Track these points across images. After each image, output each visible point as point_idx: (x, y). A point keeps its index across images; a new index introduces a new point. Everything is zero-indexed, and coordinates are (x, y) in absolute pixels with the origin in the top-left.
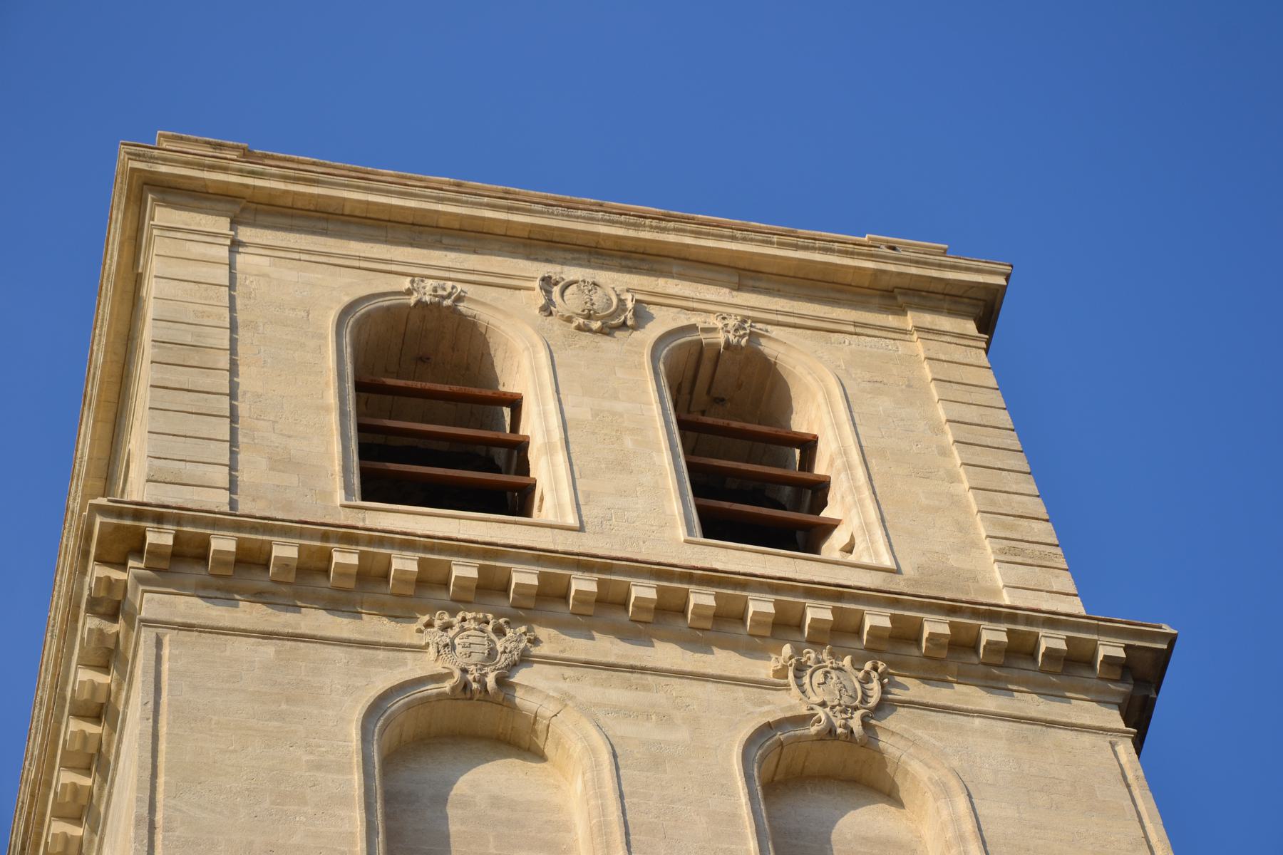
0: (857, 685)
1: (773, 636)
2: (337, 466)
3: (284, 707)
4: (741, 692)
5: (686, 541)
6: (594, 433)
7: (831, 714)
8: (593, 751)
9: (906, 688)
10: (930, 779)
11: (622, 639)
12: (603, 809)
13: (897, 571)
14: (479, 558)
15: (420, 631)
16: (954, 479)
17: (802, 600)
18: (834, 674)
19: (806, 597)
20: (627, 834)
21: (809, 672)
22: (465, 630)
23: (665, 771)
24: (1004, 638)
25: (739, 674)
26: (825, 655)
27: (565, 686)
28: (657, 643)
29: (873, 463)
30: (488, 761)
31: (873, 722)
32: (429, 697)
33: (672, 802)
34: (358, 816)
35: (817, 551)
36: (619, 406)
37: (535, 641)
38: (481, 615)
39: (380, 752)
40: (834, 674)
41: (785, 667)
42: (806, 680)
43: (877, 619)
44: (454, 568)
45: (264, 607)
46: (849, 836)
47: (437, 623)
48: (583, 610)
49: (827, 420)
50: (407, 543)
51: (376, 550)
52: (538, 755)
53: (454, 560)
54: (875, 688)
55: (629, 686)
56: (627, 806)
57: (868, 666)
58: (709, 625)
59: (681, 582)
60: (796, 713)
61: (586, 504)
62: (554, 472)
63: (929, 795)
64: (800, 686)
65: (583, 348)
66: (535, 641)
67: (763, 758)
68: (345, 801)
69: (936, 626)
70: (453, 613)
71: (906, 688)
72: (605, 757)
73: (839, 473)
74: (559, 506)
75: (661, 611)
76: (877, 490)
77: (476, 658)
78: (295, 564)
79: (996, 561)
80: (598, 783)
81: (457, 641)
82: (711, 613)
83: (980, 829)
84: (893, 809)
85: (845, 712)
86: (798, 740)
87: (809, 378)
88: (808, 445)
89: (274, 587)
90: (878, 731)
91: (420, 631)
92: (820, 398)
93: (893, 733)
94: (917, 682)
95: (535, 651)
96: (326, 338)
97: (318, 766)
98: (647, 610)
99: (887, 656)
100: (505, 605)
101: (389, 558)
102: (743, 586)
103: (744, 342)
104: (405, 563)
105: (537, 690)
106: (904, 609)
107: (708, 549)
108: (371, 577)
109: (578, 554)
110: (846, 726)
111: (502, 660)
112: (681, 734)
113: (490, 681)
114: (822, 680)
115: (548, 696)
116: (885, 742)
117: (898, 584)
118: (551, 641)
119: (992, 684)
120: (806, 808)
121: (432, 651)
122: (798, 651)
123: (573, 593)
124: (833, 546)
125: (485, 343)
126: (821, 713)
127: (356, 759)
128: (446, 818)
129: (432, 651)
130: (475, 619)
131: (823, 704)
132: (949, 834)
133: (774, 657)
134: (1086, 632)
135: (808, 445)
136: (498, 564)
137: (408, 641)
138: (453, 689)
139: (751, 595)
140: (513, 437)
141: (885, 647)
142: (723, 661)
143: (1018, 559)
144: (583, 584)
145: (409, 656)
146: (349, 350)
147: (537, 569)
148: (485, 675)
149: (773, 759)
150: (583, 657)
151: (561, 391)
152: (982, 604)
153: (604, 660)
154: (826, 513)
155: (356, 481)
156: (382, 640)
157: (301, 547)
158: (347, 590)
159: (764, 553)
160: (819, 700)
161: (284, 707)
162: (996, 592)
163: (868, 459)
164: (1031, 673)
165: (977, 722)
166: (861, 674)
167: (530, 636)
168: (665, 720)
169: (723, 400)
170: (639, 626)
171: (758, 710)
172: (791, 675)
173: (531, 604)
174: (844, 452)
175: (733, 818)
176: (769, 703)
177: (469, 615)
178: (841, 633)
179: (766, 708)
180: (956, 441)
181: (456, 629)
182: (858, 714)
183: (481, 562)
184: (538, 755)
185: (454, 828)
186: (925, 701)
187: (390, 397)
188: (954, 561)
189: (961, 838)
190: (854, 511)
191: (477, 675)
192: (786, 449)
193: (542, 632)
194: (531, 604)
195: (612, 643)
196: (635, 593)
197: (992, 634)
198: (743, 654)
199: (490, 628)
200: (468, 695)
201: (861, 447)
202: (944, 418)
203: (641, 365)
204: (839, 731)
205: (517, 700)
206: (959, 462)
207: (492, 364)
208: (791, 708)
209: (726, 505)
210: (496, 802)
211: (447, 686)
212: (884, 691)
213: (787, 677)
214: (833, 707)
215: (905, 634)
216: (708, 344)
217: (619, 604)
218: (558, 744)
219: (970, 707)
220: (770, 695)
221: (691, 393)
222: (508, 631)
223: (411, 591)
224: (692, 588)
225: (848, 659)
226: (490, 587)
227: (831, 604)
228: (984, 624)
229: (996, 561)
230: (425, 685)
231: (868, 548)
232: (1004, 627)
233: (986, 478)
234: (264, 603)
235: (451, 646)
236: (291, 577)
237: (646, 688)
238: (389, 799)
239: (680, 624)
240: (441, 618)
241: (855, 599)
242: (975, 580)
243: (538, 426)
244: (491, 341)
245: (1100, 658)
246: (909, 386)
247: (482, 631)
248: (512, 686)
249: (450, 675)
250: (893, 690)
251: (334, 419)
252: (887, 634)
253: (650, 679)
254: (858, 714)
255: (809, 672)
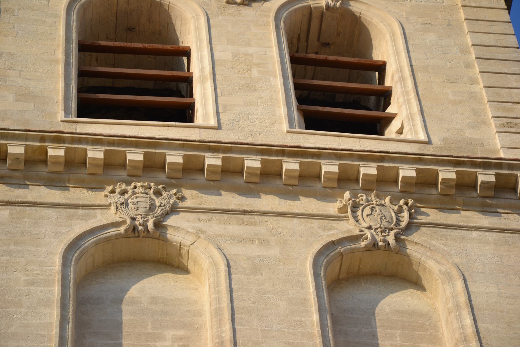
0: (393, 215)
1: (339, 187)
2: (60, 97)
3: (12, 247)
4: (316, 223)
5: (288, 132)
6: (233, 68)
7: (374, 233)
8: (215, 264)
9: (428, 215)
10: (440, 271)
11: (240, 195)
12: (219, 300)
13: (429, 142)
14: (144, 148)
15: (106, 196)
16: (473, 81)
17: (280, 158)
18: (378, 208)
19: (360, 161)
20: (233, 314)
21: (361, 208)
22: (135, 194)
23: (262, 275)
24: (493, 179)
25: (315, 212)
26: (373, 197)
27: (199, 225)
28: (263, 196)
29: (419, 76)
30: (151, 276)
31: (403, 237)
32: (110, 237)
33: (265, 293)
34: (55, 313)
35: (382, 134)
36: (251, 50)
37: (182, 199)
38: (146, 184)
39: (326, 283)
40: (378, 208)
41: (345, 206)
42: (359, 213)
43: (408, 172)
44: (88, 152)
45: (4, 186)
46: (387, 311)
47: (118, 190)
48: (214, 177)
49: (391, 51)
50: (97, 140)
51: (76, 146)
52: (183, 270)
53: (128, 150)
54: (405, 216)
55: (242, 223)
56: (234, 297)
57: (402, 202)
58: (296, 182)
59: (277, 156)
60: (351, 234)
61: (224, 112)
62: (204, 94)
63: (439, 281)
64: (355, 217)
65: (230, 15)
66: (182, 199)
67: (328, 263)
68: (48, 304)
69: (447, 174)
70: (128, 183)
71: (428, 215)
72: (223, 267)
73: (396, 84)
74: (206, 115)
75: (264, 174)
76: (420, 93)
77: (141, 211)
78: (23, 158)
79: (497, 132)
80: (216, 284)
81: (129, 201)
82: (297, 174)
83: (470, 301)
84: (418, 292)
85: (384, 231)
86: (353, 251)
87: (381, 24)
88: (381, 68)
89: (10, 173)
90: (406, 242)
91: (106, 196)
92: (388, 37)
93: (416, 243)
94: (436, 211)
95: (181, 204)
96: (59, 17)
97: (32, 283)
98: (255, 175)
99: (415, 196)
100: (162, 177)
101: (85, 150)
102: (318, 156)
103: (338, 4)
104: (96, 153)
105: (181, 229)
106: (425, 164)
107: (302, 136)
108: (74, 163)
109: (209, 142)
110: (384, 241)
111: (159, 211)
112: (274, 251)
113: (150, 225)
114: (369, 212)
115: (188, 232)
116: (412, 250)
117: (429, 150)
118: (192, 197)
119: (486, 209)
120: (356, 296)
121: (113, 207)
122: (354, 195)
123: (479, 183)
124: (391, 131)
125: (169, 16)
126: (368, 233)
127: (58, 277)
128: (121, 312)
129: (113, 207)
130: (142, 186)
131: (370, 228)
132: (450, 305)
133: (339, 199)
134: (429, 165)
135: (381, 68)
136: (157, 151)
137: (98, 202)
138: (126, 231)
139: (323, 161)
140: (380, 87)
141: (413, 190)
142: (306, 204)
143: (513, 130)
144: (213, 160)
145: (98, 212)
146: (75, 24)
147: (182, 153)
148: (147, 221)
149: (336, 265)
150: (213, 206)
151: (213, 43)
152: (478, 158)
153: (226, 208)
154: (389, 110)
155: (74, 105)
156: (81, 203)
157: (26, 147)
158: (59, 173)
159: (339, 136)
160: (366, 225)
161: (12, 247)
162: (498, 151)
163: (416, 73)
164: (513, 201)
165: (475, 234)
166: (396, 208)
167: (179, 195)
168: (264, 243)
169: (328, 44)
170: (251, 185)
171: (327, 233)
172: (349, 210)
173: (180, 175)
174: (400, 70)
175: (305, 300)
176: (334, 229)
177: (138, 184)
178: (384, 182)
179: (332, 232)
180: (477, 58)
181: (130, 193)
182: (392, 233)
183: (146, 150)
184: (183, 270)
185: (125, 318)
186: (439, 222)
187: (112, 55)
188: (469, 134)
189: (458, 307)
190: (404, 107)
191: (141, 221)
192: (176, 58)
193: (187, 193)
194: (180, 175)
195: (233, 197)
196: (402, 173)
197: (486, 177)
198: (319, 200)
199: (151, 191)
200: (137, 235)
201: (411, 66)
202: (470, 44)
203: (268, 23)
204: (380, 244)
205: (168, 236)
206: (478, 71)
207: (175, 29)
208: (348, 231)
209: (320, 108)
210: (154, 300)
211: (122, 229)
212: (411, 216)
213: (347, 212)
214: (376, 229)
215: (426, 182)
216: (315, 8)
217: (511, 189)
218: (195, 262)
219: (470, 225)
220: (335, 224)
221: (307, 41)
222: (163, 192)
223: (100, 171)
224: (284, 159)
225: (388, 199)
226: (153, 166)
227: (376, 164)
228: (479, 171)
229: (497, 132)
230: (107, 229)
231: (411, 130)
232: (493, 172)
233: (495, 80)
234: (4, 184)
235: (126, 204)
236: (21, 167)
237: (253, 224)
238: (81, 303)
239: (278, 183)
240: (121, 187)
241: (393, 160)
242: (482, 145)
243: (199, 67)
244: (172, 14)
245: (479, 183)
246: (448, 25)
247: (146, 194)
248: (165, 227)
249: (124, 222)
250: (419, 217)
251: (60, 68)
252: (414, 181)
253: (256, 218)
254: (392, 233)
255: (361, 208)
